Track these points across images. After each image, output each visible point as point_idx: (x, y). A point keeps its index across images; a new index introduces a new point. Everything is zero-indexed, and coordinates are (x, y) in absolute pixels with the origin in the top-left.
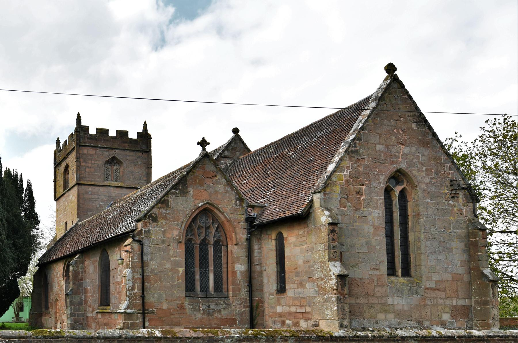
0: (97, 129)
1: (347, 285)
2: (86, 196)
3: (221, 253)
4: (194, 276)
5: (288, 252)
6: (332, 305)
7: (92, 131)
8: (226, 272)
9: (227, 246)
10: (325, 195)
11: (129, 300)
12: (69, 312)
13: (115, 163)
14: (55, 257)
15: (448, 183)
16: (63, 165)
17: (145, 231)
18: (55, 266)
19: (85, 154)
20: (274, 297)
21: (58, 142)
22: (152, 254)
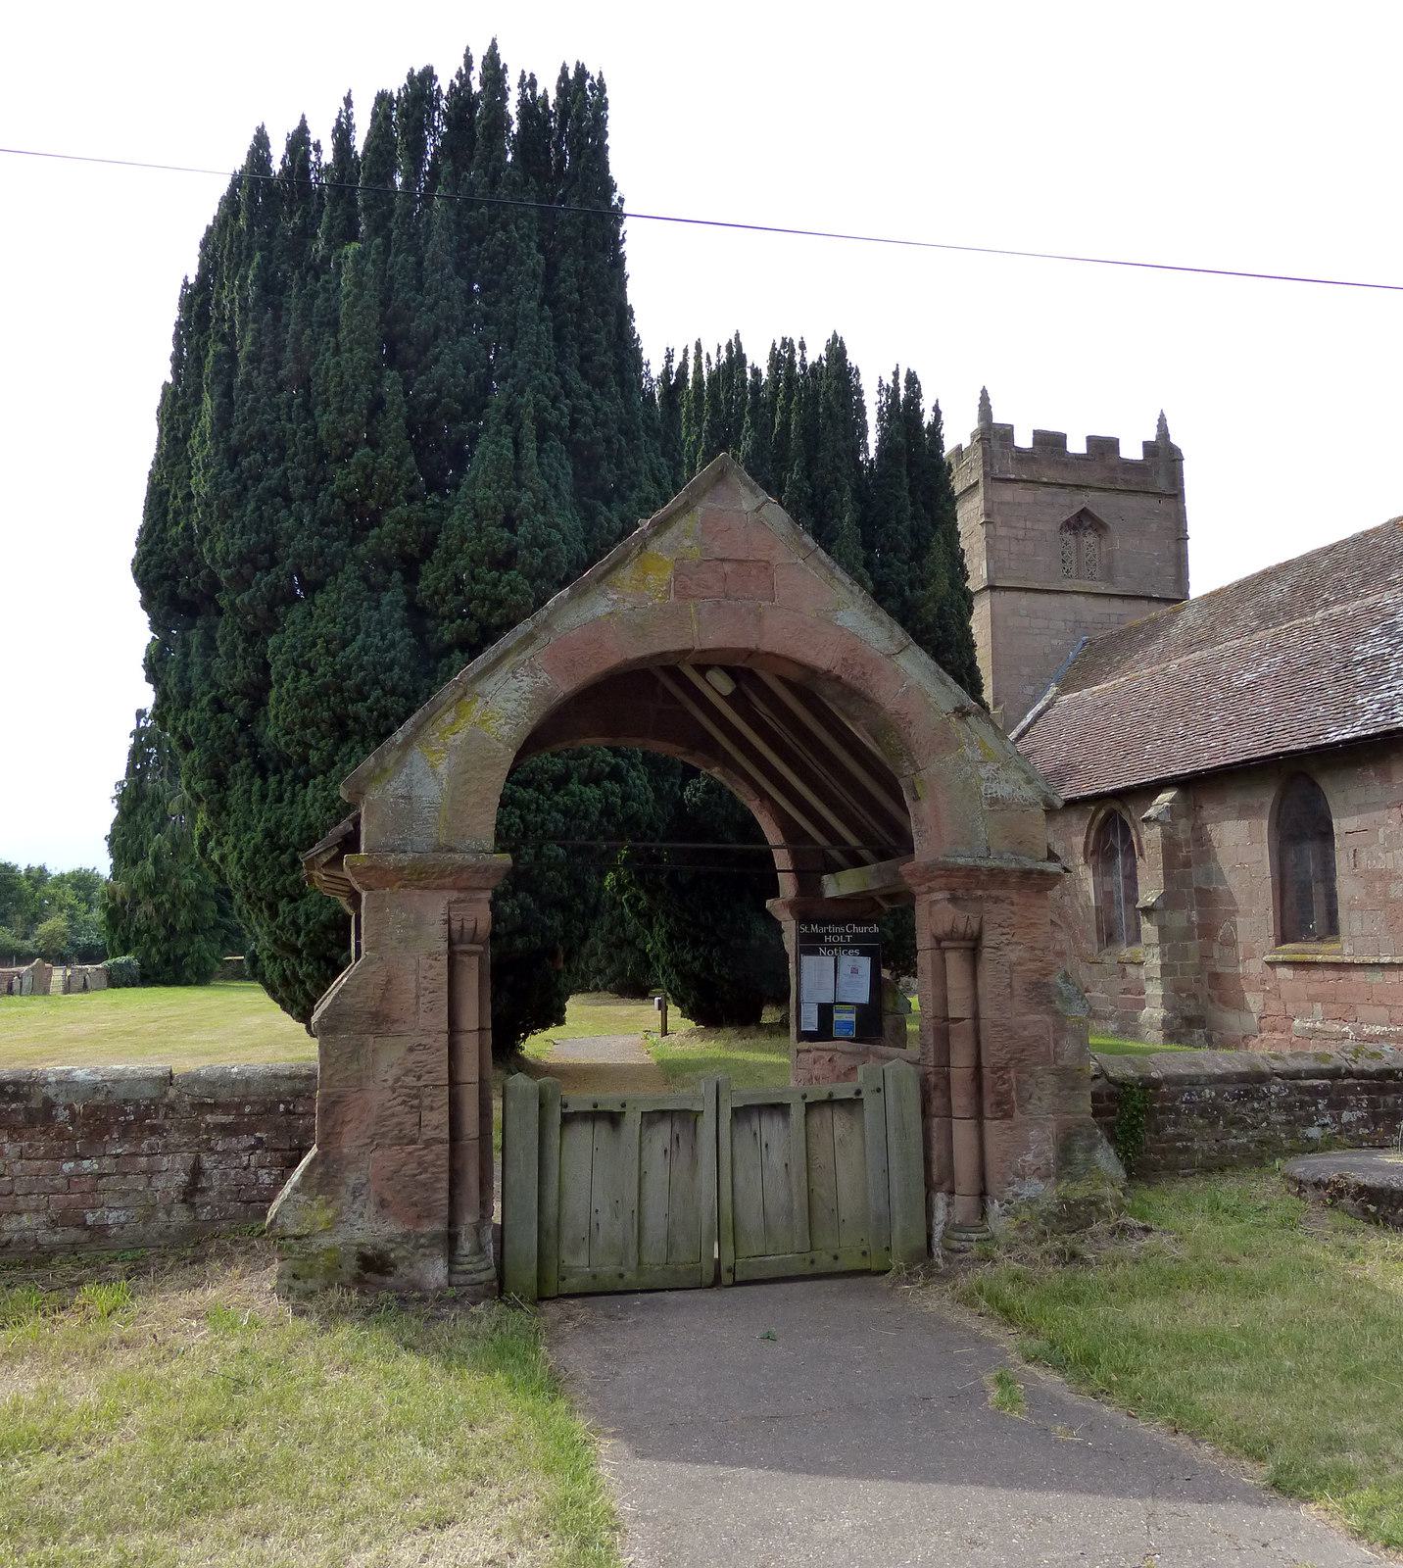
0: (1035, 433)
7: (1023, 440)
13: (1086, 529)
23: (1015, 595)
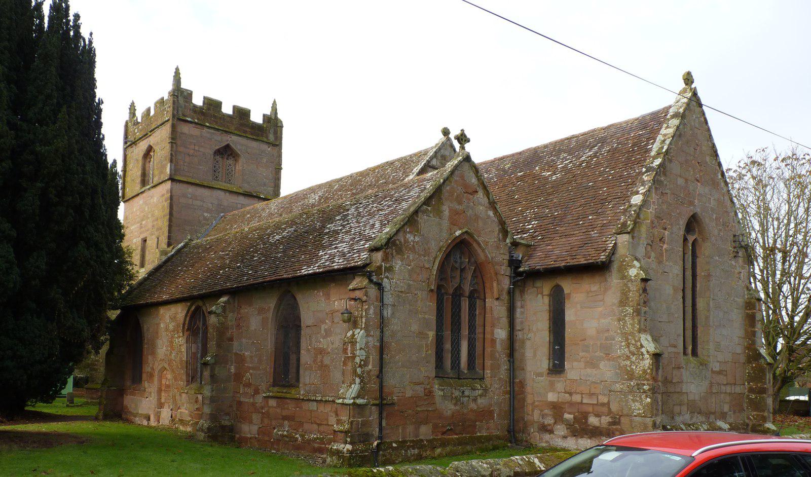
0: (205, 98)
1: (661, 367)
2: (182, 200)
3: (476, 309)
4: (443, 344)
5: (570, 315)
6: (643, 396)
7: (198, 101)
8: (482, 340)
9: (485, 301)
10: (633, 237)
11: (360, 384)
12: (209, 394)
13: (228, 155)
14: (165, 297)
15: (732, 237)
16: (143, 146)
17: (385, 267)
18: (160, 308)
19: (185, 134)
20: (544, 380)
21: (132, 109)
22: (394, 305)
23: (185, 185)
